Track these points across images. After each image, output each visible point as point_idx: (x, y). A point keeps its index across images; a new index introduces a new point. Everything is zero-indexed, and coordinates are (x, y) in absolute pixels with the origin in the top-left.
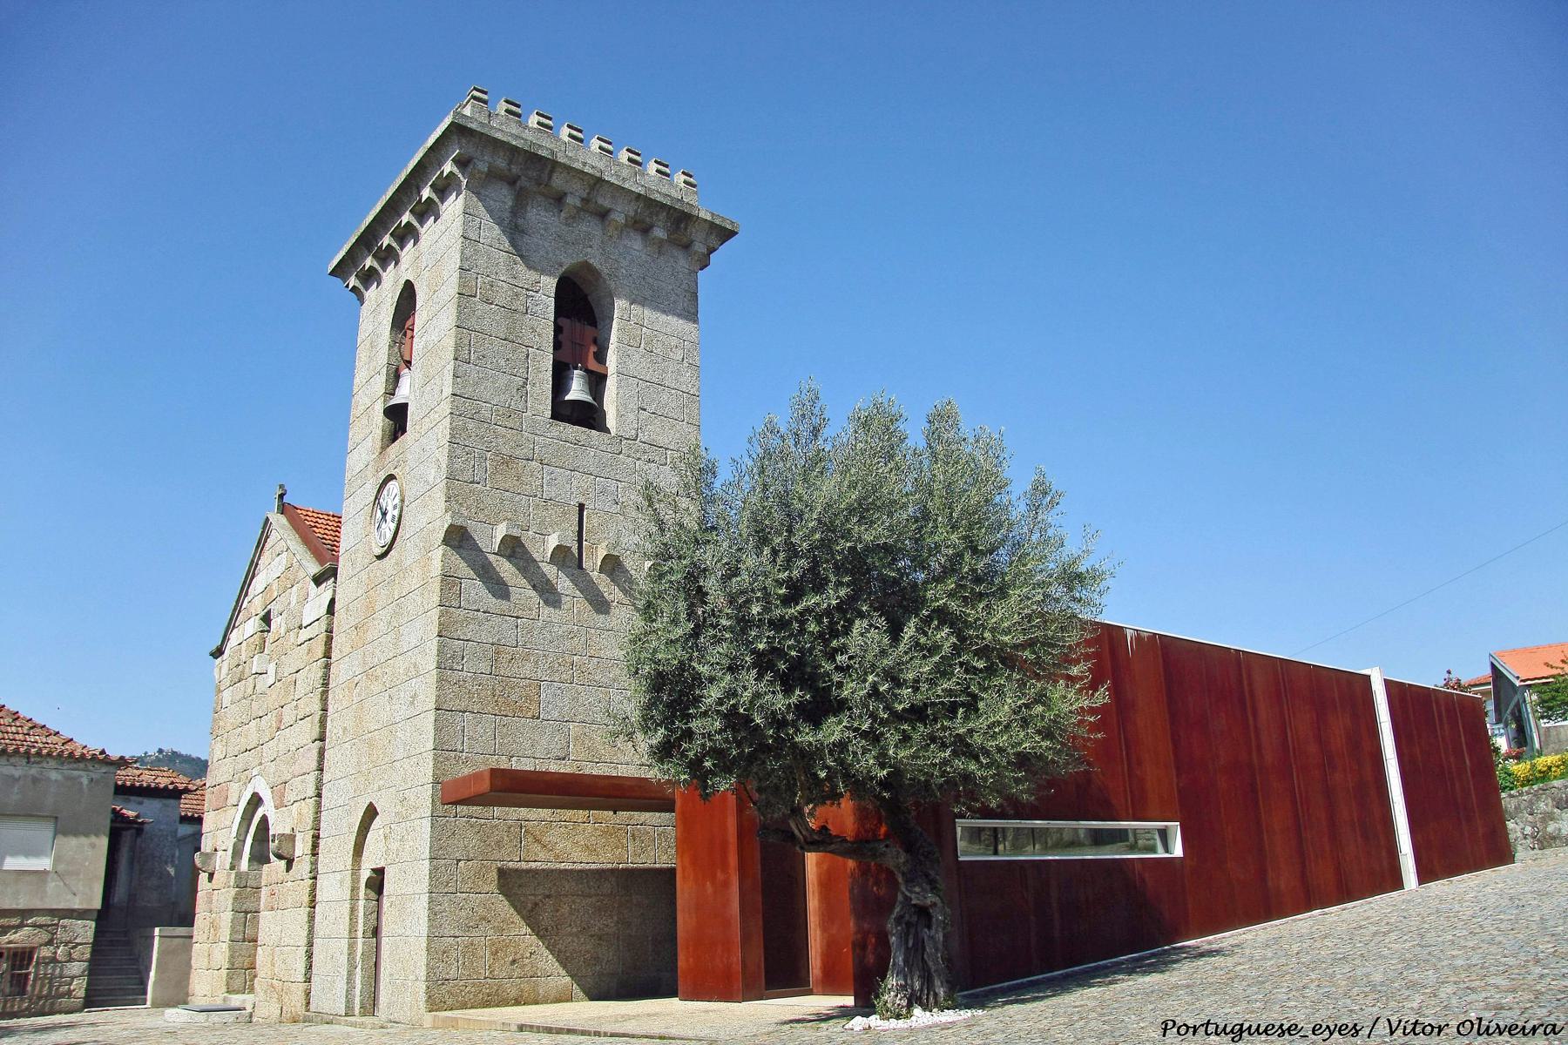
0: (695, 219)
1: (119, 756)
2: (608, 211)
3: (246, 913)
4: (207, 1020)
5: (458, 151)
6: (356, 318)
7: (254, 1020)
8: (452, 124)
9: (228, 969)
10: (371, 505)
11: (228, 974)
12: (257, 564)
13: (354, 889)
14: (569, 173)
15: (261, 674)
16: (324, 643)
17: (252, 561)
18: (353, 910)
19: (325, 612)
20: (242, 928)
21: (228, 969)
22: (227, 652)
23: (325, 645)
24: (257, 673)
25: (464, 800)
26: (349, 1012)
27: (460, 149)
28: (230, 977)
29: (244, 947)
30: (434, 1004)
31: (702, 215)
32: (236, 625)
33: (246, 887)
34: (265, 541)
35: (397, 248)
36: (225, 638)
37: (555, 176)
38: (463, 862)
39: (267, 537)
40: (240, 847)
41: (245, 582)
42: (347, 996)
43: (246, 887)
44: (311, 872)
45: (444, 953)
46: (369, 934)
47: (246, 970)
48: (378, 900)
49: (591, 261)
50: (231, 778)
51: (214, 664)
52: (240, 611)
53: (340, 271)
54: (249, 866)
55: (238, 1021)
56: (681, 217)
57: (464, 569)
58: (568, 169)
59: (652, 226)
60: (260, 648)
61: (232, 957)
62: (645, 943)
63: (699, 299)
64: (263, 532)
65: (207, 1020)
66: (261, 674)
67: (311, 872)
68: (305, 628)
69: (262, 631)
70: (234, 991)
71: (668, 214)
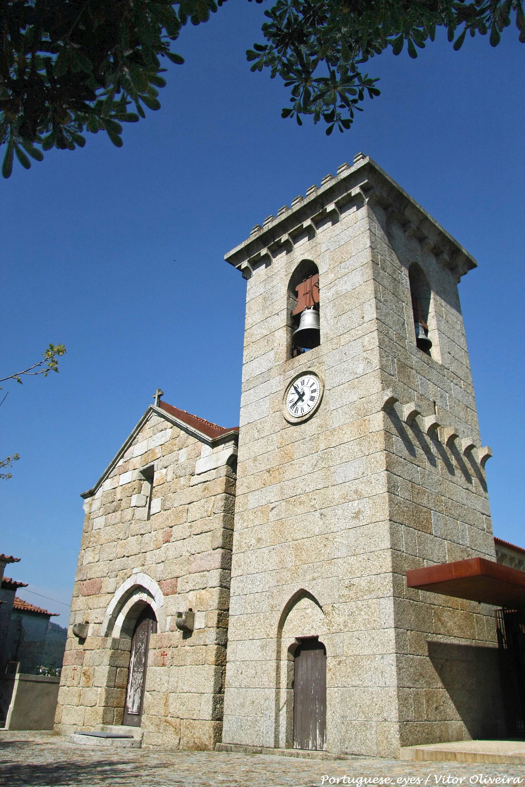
0: (461, 253)
1: (9, 556)
2: (426, 238)
3: (117, 667)
4: (112, 744)
5: (367, 181)
6: (246, 286)
7: (143, 746)
8: (368, 165)
9: (104, 706)
10: (282, 393)
11: (104, 710)
12: (135, 438)
13: (279, 652)
14: (413, 210)
15: (138, 507)
16: (224, 483)
17: (132, 436)
18: (278, 668)
19: (225, 463)
20: (114, 678)
21: (104, 706)
22: (98, 494)
23: (225, 485)
24: (135, 506)
25: (438, 583)
26: (277, 746)
27: (368, 180)
28: (105, 713)
29: (114, 691)
30: (405, 742)
31: (464, 251)
32: (110, 476)
33: (118, 649)
34: (145, 423)
35: (292, 242)
36: (99, 485)
37: (407, 209)
38: (409, 631)
39: (147, 421)
40: (113, 621)
41: (123, 449)
42: (275, 732)
43: (118, 649)
44: (216, 640)
45: (406, 700)
46: (290, 686)
47: (115, 708)
48: (294, 661)
49: (419, 263)
50: (105, 575)
51: (83, 501)
52: (114, 468)
53: (234, 260)
54: (121, 635)
55: (133, 746)
56: (456, 251)
57: (394, 430)
58: (414, 207)
59: (442, 252)
60: (139, 490)
61: (107, 698)
62: (348, 699)
63: (460, 299)
64: (145, 417)
65: (112, 744)
66: (138, 507)
67: (216, 640)
68: (198, 475)
69: (140, 480)
70: (107, 723)
71: (450, 247)
